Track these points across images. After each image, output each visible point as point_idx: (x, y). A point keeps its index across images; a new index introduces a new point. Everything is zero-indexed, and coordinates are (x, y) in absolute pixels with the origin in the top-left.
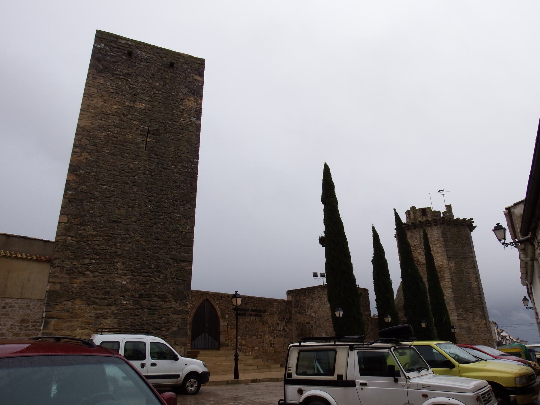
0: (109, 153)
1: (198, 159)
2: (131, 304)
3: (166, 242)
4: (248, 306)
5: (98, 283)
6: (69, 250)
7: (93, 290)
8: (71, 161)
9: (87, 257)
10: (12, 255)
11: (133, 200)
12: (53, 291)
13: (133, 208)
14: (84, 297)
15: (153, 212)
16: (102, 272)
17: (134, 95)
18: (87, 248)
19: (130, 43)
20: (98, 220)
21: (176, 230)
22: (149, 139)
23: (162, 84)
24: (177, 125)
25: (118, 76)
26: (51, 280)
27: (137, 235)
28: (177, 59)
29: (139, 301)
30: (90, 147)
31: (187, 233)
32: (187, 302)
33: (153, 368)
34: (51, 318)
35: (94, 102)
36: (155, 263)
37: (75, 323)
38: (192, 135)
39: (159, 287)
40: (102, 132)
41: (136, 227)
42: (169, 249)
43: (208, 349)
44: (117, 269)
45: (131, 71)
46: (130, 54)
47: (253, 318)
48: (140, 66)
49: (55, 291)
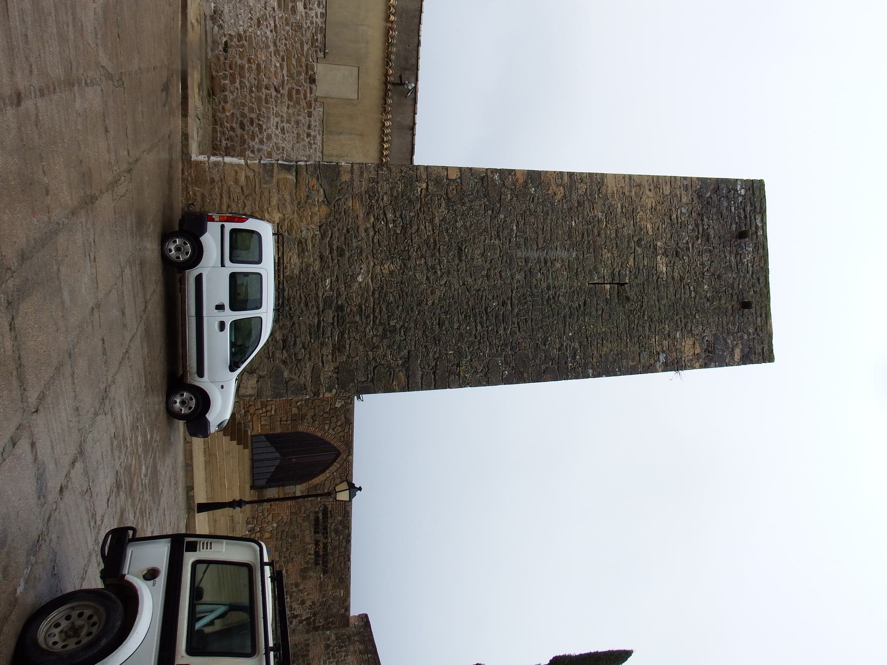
0: (570, 227)
1: (594, 376)
2: (326, 294)
3: (436, 340)
4: (333, 535)
5: (356, 237)
6: (406, 187)
7: (345, 231)
8: (547, 172)
9: (398, 215)
10: (387, 135)
11: (501, 276)
12: (339, 172)
13: (488, 276)
14: (332, 218)
15: (486, 309)
16: (375, 241)
17: (677, 252)
18: (412, 214)
19: (760, 233)
20: (459, 225)
21: (459, 354)
22: (608, 287)
23: (708, 295)
24: (644, 331)
25: (700, 222)
26: (355, 167)
27: (443, 289)
28: (758, 313)
29: (330, 306)
30: (574, 196)
31: (459, 375)
32: (334, 391)
33: (216, 326)
34: (297, 174)
35: (648, 192)
36: (398, 326)
37: (289, 210)
38: (633, 360)
39: (358, 337)
40: (602, 212)
41: (457, 287)
42: (426, 347)
43: (253, 468)
44: (382, 264)
45: (715, 241)
46: (742, 235)
47: (311, 548)
48: (727, 255)
49: (338, 174)
